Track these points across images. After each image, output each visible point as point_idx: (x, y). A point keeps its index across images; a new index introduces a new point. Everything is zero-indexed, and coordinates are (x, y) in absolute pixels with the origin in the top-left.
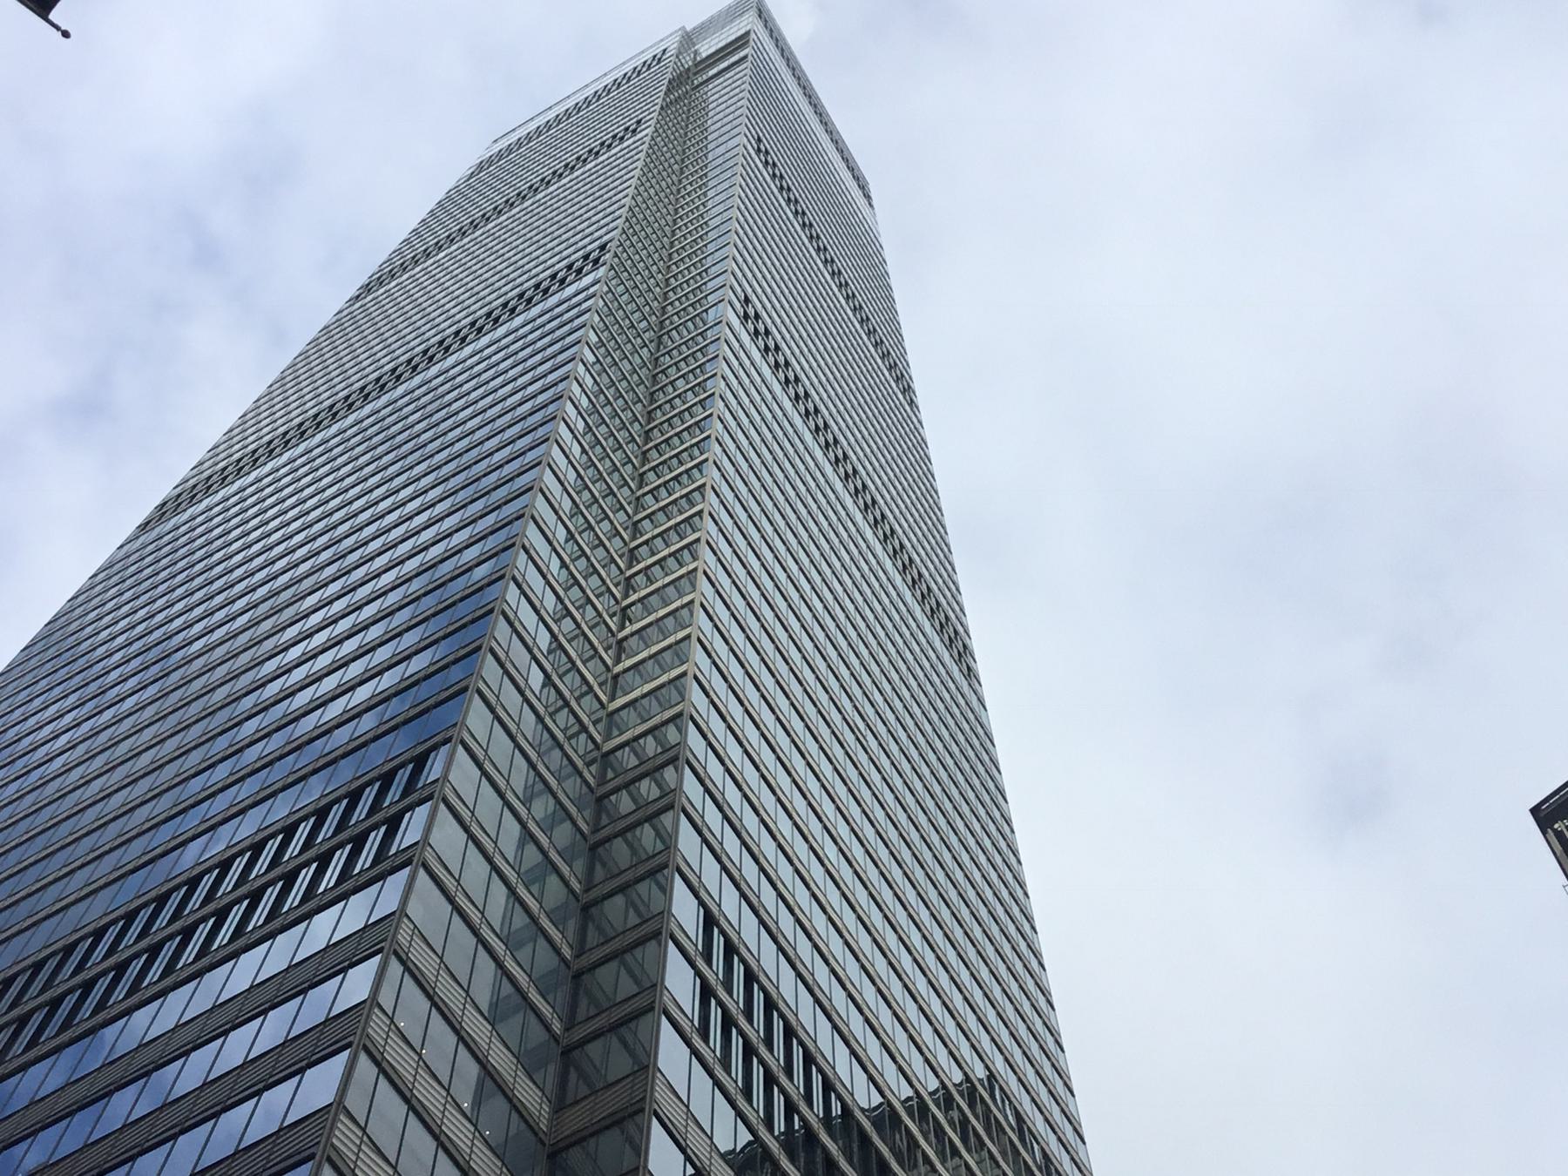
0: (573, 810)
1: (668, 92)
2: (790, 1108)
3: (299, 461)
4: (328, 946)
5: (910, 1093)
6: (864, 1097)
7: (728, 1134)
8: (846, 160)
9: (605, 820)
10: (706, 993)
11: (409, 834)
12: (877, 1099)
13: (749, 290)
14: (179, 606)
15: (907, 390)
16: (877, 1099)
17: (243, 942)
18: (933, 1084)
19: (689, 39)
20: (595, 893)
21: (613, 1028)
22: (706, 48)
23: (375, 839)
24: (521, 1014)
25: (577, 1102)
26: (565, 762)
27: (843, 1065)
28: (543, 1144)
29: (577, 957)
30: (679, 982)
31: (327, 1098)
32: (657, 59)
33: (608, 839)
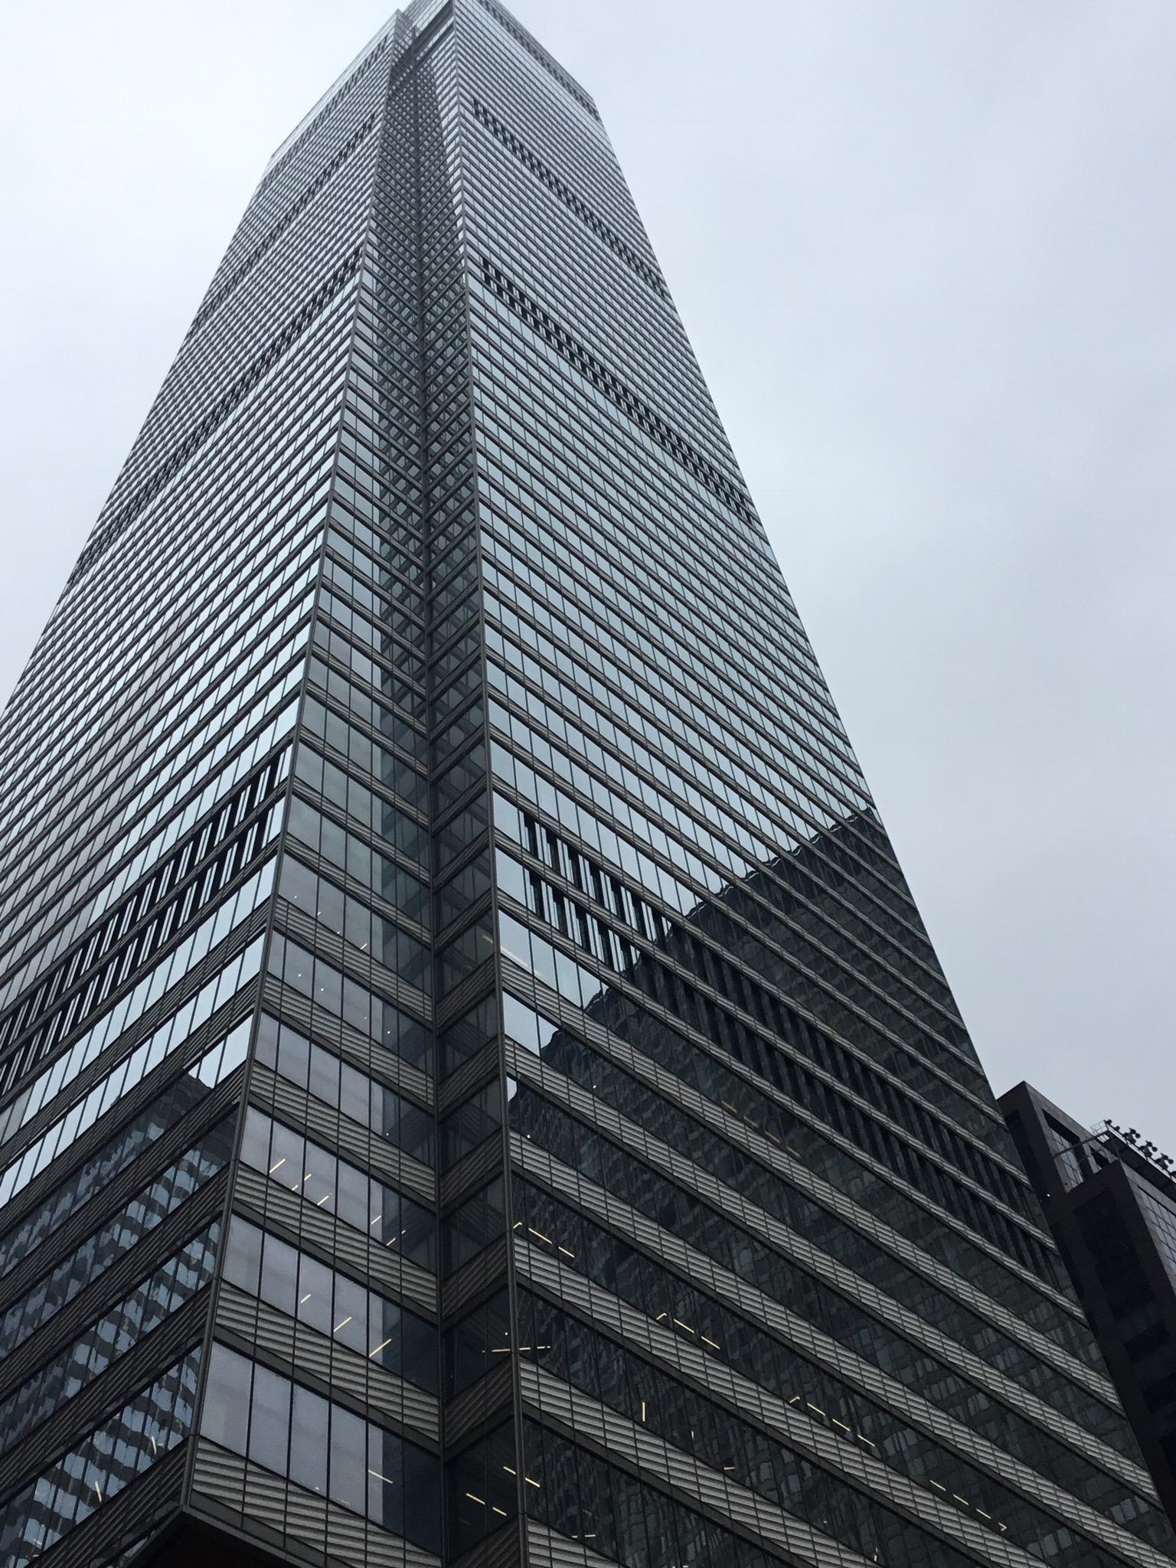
0: (410, 760)
1: (391, 83)
2: (626, 944)
3: (253, 408)
4: (189, 1036)
7: (579, 987)
9: (440, 757)
10: (536, 879)
11: (274, 828)
13: (486, 252)
14: (156, 552)
15: (658, 283)
17: (221, 895)
19: (403, 20)
20: (440, 821)
21: (471, 861)
22: (422, 23)
23: (252, 835)
24: (394, 940)
25: (455, 1071)
26: (398, 722)
27: (649, 876)
28: (433, 1117)
29: (435, 937)
30: (510, 878)
31: (242, 1057)
32: (381, 47)
33: (443, 732)
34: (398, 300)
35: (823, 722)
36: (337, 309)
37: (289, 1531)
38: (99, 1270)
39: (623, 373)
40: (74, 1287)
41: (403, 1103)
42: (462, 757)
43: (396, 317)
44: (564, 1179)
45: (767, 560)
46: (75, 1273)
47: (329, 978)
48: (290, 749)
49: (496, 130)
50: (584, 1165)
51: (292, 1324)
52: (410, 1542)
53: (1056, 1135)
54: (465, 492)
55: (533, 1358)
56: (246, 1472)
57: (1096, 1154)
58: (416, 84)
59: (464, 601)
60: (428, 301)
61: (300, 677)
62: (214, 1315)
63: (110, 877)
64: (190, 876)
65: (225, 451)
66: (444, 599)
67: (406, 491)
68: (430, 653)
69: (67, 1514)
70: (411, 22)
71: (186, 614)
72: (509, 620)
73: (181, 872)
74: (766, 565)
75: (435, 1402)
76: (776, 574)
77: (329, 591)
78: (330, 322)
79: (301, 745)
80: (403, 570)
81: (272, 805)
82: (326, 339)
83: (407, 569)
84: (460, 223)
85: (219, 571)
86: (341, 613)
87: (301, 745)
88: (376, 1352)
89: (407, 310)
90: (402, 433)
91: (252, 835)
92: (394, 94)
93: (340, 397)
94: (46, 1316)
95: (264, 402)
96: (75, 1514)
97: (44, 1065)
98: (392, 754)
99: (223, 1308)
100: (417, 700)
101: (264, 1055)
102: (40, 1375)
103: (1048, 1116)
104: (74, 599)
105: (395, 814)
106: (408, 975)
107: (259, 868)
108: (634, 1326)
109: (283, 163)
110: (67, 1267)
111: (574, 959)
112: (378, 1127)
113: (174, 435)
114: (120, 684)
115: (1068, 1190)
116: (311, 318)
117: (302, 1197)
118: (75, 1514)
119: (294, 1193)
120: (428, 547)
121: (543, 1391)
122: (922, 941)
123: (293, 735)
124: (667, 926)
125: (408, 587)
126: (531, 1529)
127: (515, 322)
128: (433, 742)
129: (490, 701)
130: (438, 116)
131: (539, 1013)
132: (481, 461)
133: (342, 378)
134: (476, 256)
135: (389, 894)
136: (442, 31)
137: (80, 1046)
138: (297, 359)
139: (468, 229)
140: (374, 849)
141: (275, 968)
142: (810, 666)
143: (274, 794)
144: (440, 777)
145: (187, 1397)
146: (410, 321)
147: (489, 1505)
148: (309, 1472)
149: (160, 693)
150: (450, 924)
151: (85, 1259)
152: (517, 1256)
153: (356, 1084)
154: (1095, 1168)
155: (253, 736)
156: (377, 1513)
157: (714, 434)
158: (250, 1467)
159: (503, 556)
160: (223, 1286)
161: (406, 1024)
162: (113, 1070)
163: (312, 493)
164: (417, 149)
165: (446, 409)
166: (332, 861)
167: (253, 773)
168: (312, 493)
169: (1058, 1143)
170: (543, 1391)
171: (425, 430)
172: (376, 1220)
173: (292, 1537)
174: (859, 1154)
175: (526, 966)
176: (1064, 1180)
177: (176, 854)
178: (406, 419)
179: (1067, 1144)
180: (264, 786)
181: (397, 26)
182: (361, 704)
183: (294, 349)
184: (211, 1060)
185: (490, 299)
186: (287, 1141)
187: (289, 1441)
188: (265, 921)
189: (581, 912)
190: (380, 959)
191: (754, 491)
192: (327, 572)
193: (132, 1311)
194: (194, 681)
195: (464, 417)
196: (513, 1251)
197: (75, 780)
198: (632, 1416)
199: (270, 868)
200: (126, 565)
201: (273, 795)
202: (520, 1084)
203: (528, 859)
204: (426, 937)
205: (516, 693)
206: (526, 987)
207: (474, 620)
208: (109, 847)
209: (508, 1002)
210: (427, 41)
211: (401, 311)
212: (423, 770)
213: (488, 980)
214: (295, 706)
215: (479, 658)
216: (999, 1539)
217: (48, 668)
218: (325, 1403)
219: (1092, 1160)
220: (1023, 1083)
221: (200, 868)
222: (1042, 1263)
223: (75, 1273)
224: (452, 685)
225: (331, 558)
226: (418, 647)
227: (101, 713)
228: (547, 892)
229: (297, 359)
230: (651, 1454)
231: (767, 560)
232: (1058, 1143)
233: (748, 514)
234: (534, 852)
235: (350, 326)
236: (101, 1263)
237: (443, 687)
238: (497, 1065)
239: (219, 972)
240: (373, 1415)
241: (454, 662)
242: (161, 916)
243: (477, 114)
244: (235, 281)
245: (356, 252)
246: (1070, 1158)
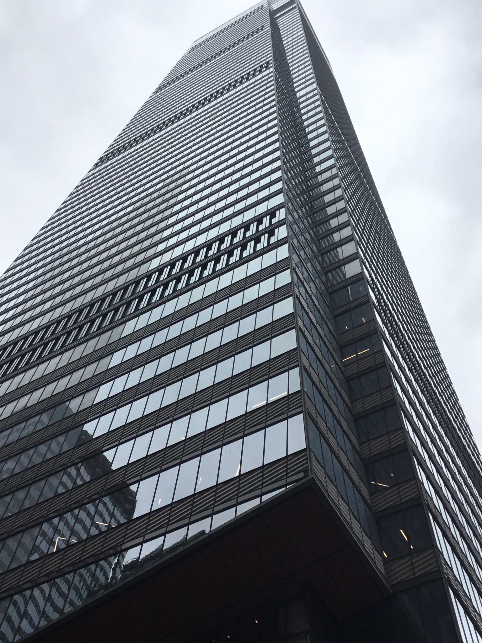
3: (96, 174)
36: (137, 150)
64: (19, 354)
65: (85, 185)
73: (15, 351)
78: (133, 154)
82: (135, 157)
95: (96, 177)
116: (131, 146)
136: (281, 13)
138: (127, 157)
155: (95, 287)
167: (27, 335)
183: (109, 163)
184: (78, 400)
221: (13, 358)
229: (121, 161)
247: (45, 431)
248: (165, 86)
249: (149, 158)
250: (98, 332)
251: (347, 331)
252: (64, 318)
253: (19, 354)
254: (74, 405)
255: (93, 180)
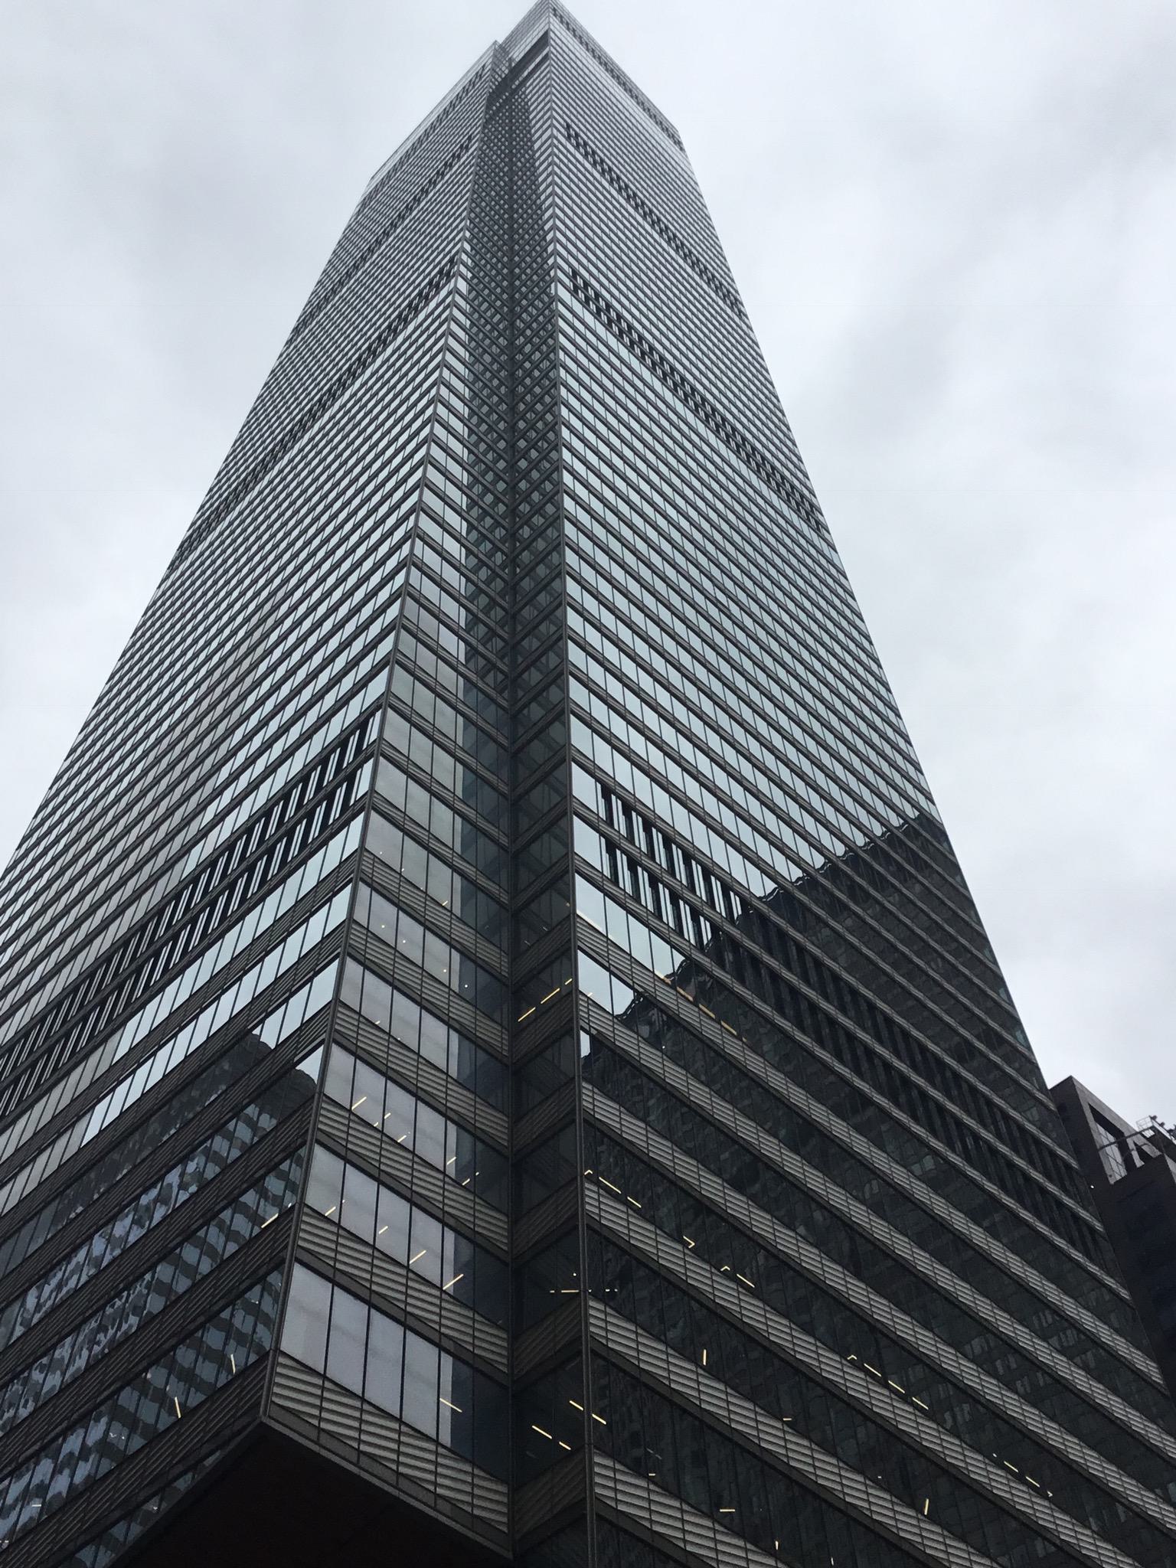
0: (493, 732)
1: (488, 107)
5: (800, 874)
6: (760, 886)
8: (653, 117)
10: (611, 847)
11: (362, 786)
12: (770, 886)
15: (735, 303)
16: (770, 886)
17: (309, 850)
18: (819, 861)
19: (501, 51)
22: (518, 54)
23: (340, 794)
30: (587, 844)
31: (328, 997)
32: (479, 76)
34: (491, 306)
35: (885, 720)
37: (363, 1448)
38: (183, 1196)
39: (702, 384)
40: (159, 1213)
41: (478, 1143)
42: (541, 732)
43: (485, 403)
44: (633, 1130)
45: (834, 566)
46: (162, 1199)
47: (407, 1009)
48: (378, 714)
49: (587, 153)
50: (652, 1118)
51: (370, 1251)
52: (479, 1467)
53: (1101, 1130)
54: (550, 509)
55: (596, 1297)
56: (323, 1388)
57: (1139, 1149)
58: (511, 117)
59: (545, 586)
60: (518, 309)
61: (382, 689)
62: (296, 1237)
63: (203, 834)
64: (243, 866)
66: (527, 584)
67: (494, 483)
68: (513, 632)
69: (150, 1420)
70: (508, 53)
71: (280, 594)
72: (596, 672)
73: (252, 847)
74: (833, 571)
75: (503, 1489)
76: (858, 622)
77: (419, 569)
79: (390, 711)
80: (490, 555)
81: (360, 766)
83: (493, 555)
84: (550, 249)
85: (295, 608)
86: (430, 590)
87: (389, 710)
88: (448, 1286)
89: (498, 316)
90: (490, 448)
91: (340, 794)
92: (491, 118)
93: (433, 392)
94: (132, 1239)
96: (157, 1421)
97: (136, 1007)
98: (475, 686)
99: (281, 1375)
100: (500, 677)
101: (349, 996)
102: (125, 1294)
103: (1093, 1109)
104: (173, 584)
105: (475, 778)
106: (486, 933)
107: (347, 823)
108: (699, 1275)
109: (382, 183)
110: (154, 1193)
111: (646, 925)
112: (453, 1072)
113: (244, 530)
114: (216, 659)
115: (1112, 1182)
117: (382, 1132)
118: (157, 1421)
119: (375, 1129)
120: (513, 536)
121: (611, 1329)
122: (1008, 1012)
123: (383, 701)
124: (736, 902)
125: (493, 571)
126: (597, 1459)
127: (601, 330)
128: (514, 716)
129: (572, 717)
130: (530, 140)
131: (612, 973)
132: (564, 412)
133: (436, 375)
134: (566, 267)
135: (470, 855)
136: (538, 60)
137: (171, 990)
139: (559, 241)
140: (456, 811)
141: (360, 916)
142: (866, 644)
143: (363, 755)
144: (521, 749)
145: (267, 1321)
146: (501, 326)
147: (555, 1441)
148: (383, 1393)
149: (254, 666)
150: (529, 886)
151: (170, 1185)
152: (587, 1192)
153: (435, 1030)
154: (1139, 1163)
155: (325, 720)
156: (446, 1438)
157: (792, 462)
158: (327, 1385)
159: (588, 573)
160: (306, 1210)
161: (483, 978)
162: (203, 1010)
163: (405, 480)
164: (511, 169)
165: (533, 427)
166: (418, 799)
168: (405, 480)
169: (1103, 1136)
170: (611, 1329)
171: (513, 427)
172: (451, 1161)
173: (365, 1453)
174: (917, 1129)
175: (602, 930)
176: (1108, 1172)
177: (266, 813)
178: (489, 546)
179: (1112, 1139)
180: (356, 747)
181: (495, 56)
182: (448, 677)
184: (272, 1022)
185: (578, 308)
186: (360, 1186)
187: (368, 1364)
188: (355, 871)
189: (654, 881)
190: (455, 1076)
191: (822, 500)
192: (418, 552)
193: (213, 1235)
194: (264, 723)
195: (551, 435)
196: (583, 1195)
197: (171, 747)
198: (697, 1361)
199: (357, 824)
200: (214, 572)
201: (349, 813)
202: (593, 1040)
203: (604, 828)
204: (505, 898)
205: (591, 604)
206: (601, 947)
207: (555, 604)
208: (202, 808)
209: (584, 962)
210: (525, 67)
211: (493, 316)
212: (505, 742)
213: (564, 939)
214: (384, 675)
215: (561, 674)
216: (1046, 1503)
217: (137, 657)
218: (400, 1330)
219: (1135, 1155)
220: (1070, 1079)
222: (1090, 1245)
223: (162, 1199)
224: (534, 699)
225: (422, 539)
226: (502, 627)
227: (197, 686)
228: (622, 860)
230: (714, 1398)
231: (834, 566)
232: (1103, 1136)
233: (818, 522)
234: (610, 821)
235: (445, 327)
236: (186, 1189)
237: (524, 700)
238: (571, 1020)
239: (307, 920)
240: (445, 1343)
241: (536, 644)
242: (251, 870)
243: (569, 138)
244: (334, 292)
245: (451, 261)
246: (1113, 1153)
247: (200, 1120)
248: (312, 316)
249: (427, 357)
250: (344, 818)
251: (530, 947)
252: (333, 751)
253: (243, 866)
254: (270, 1033)
255: (346, 419)
